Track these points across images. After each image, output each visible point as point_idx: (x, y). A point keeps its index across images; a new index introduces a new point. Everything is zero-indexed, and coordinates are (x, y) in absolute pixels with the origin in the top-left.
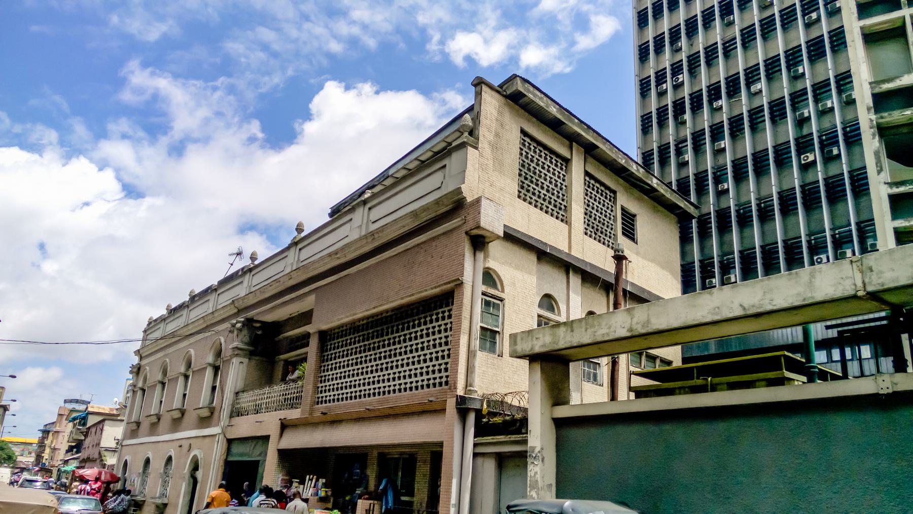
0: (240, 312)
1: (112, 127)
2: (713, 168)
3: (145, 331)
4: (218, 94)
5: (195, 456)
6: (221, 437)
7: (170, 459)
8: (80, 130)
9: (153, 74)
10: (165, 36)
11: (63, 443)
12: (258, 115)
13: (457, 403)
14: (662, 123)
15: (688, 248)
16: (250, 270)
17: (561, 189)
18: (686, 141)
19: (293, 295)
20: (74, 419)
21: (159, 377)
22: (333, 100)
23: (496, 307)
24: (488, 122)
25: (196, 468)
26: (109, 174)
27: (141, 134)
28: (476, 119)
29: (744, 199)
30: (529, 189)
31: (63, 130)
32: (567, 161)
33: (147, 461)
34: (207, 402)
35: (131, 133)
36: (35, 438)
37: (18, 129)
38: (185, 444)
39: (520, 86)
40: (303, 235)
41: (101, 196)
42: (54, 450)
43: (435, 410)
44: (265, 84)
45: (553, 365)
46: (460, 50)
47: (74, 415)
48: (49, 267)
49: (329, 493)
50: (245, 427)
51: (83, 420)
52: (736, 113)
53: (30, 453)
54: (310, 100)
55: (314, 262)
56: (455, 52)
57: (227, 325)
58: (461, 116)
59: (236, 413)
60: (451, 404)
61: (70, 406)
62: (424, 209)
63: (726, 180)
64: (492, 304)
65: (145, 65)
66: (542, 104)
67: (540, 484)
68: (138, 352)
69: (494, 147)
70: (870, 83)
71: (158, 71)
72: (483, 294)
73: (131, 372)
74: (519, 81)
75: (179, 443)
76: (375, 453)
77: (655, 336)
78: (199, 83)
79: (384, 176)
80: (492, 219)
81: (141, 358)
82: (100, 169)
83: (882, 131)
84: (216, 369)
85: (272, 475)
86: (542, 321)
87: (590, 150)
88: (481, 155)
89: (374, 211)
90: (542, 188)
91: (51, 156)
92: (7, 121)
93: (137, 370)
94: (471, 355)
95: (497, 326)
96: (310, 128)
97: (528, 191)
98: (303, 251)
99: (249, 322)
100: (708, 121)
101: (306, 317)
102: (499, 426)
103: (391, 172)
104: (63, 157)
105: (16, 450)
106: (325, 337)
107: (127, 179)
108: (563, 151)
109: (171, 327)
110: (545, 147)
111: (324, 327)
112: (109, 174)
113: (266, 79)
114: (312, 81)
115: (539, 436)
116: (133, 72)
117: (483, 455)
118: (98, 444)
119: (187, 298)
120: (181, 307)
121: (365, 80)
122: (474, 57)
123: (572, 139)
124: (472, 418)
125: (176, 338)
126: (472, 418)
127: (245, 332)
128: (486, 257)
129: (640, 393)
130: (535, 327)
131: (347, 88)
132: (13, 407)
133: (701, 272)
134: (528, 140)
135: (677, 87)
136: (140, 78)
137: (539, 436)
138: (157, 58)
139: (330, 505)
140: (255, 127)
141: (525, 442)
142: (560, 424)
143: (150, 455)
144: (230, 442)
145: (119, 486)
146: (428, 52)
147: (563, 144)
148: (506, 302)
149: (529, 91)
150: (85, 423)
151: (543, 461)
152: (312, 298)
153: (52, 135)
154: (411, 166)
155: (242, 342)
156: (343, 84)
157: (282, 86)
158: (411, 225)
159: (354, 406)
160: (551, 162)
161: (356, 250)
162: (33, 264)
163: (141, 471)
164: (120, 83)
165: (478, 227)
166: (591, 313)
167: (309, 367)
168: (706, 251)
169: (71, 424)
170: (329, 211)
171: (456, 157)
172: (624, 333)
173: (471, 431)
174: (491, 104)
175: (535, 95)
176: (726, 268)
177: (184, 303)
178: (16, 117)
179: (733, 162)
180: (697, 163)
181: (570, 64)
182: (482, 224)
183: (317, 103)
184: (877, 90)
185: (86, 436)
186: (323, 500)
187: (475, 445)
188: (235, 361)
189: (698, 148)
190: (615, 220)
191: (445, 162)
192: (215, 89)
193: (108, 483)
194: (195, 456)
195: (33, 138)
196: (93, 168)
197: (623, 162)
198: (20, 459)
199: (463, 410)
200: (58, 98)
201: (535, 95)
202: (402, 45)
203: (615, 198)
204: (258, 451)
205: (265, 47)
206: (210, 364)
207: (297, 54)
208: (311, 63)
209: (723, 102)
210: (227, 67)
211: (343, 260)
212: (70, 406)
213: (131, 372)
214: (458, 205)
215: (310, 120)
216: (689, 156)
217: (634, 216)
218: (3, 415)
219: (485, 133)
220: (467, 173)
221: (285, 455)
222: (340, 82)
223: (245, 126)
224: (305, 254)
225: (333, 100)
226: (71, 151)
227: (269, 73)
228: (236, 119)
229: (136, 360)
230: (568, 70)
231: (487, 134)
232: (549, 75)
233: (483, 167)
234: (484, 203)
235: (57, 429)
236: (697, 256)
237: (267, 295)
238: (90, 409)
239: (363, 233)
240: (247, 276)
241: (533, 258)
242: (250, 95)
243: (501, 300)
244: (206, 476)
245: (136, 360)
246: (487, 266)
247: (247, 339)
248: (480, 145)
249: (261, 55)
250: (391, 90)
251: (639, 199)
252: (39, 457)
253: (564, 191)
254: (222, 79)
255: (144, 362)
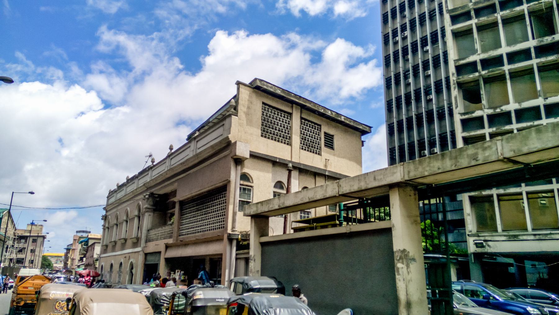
0: (148, 189)
1: (93, 67)
2: (424, 86)
3: (108, 197)
4: (154, 43)
5: (131, 262)
6: (142, 253)
7: (121, 264)
8: (75, 69)
9: (115, 34)
10: (120, 9)
11: (77, 256)
12: (178, 54)
13: (228, 236)
14: (396, 60)
15: (443, 123)
16: (151, 168)
17: (287, 128)
18: (409, 71)
19: (168, 182)
20: (81, 242)
21: (125, 218)
22: (222, 43)
23: (249, 190)
24: (243, 102)
25: (132, 268)
26: (93, 94)
27: (111, 70)
28: (237, 102)
29: (441, 105)
30: (267, 131)
31: (66, 70)
32: (291, 114)
33: (112, 265)
34: (136, 235)
35: (104, 70)
36: (62, 253)
37: (39, 70)
38: (127, 256)
39: (258, 83)
40: (173, 151)
41: (90, 109)
42: (73, 260)
43: (219, 239)
44: (181, 35)
45: (261, 220)
46: (297, 6)
47: (82, 240)
48: (65, 152)
49: (186, 278)
50: (152, 247)
51: (86, 242)
52: (437, 54)
53: (61, 262)
54: (208, 42)
55: (175, 167)
56: (294, 7)
57: (141, 196)
58: (230, 101)
59: (148, 240)
60: (226, 237)
61: (80, 235)
62: (216, 145)
63: (431, 94)
64: (246, 190)
65: (110, 28)
66: (272, 90)
67: (253, 270)
68: (104, 209)
69: (247, 114)
70: (454, 61)
71: (117, 32)
72: (241, 185)
73: (102, 219)
74: (258, 81)
75: (124, 256)
76: (208, 258)
77: (536, 153)
78: (142, 37)
79: (208, 122)
80: (242, 151)
81: (107, 212)
82: (88, 92)
83: (460, 85)
84: (139, 217)
85: (163, 271)
86: (275, 194)
87: (303, 107)
88: (240, 119)
89: (199, 143)
90: (276, 129)
91: (58, 86)
92: (33, 66)
93: (105, 218)
94: (234, 214)
95: (250, 199)
96: (209, 61)
97: (267, 132)
98: (173, 160)
99: (152, 195)
100: (421, 59)
101: (174, 193)
102: (242, 245)
103: (211, 120)
104: (66, 86)
105: (53, 260)
106: (182, 203)
107: (105, 97)
108: (288, 110)
109: (120, 195)
110: (277, 109)
111: (181, 199)
112: (93, 94)
113: (181, 32)
114: (209, 32)
115: (254, 251)
116: (103, 33)
117: (240, 258)
118: (93, 256)
119: (125, 181)
120: (123, 185)
121: (240, 29)
122: (306, 10)
123: (292, 102)
124: (235, 243)
125: (120, 202)
126: (235, 243)
127: (151, 199)
128: (242, 169)
129: (296, 230)
130: (272, 197)
131: (230, 34)
132: (48, 237)
133: (419, 147)
134: (267, 107)
135: (404, 38)
136: (108, 37)
137: (254, 251)
138: (116, 23)
139: (187, 283)
140: (177, 63)
141: (248, 253)
142: (263, 244)
143: (113, 262)
144: (146, 255)
145: (100, 278)
146: (277, 9)
147: (288, 106)
148: (254, 188)
149: (264, 85)
150: (87, 245)
151: (254, 260)
152: (176, 184)
153: (60, 73)
154: (219, 117)
155: (149, 205)
156: (227, 32)
157: (191, 35)
158: (212, 152)
159: (192, 237)
160: (281, 116)
161: (192, 162)
162: (57, 151)
163: (109, 270)
164: (96, 40)
165: (236, 155)
166: (305, 188)
167: (175, 218)
168: (421, 135)
169: (80, 245)
170: (187, 137)
171: (228, 120)
172: (277, 207)
173: (234, 249)
174: (245, 93)
175: (267, 86)
176: (432, 144)
177: (135, 176)
178: (38, 63)
179: (435, 82)
180: (436, 76)
181: (365, 11)
182: (237, 154)
183: (212, 45)
184: (457, 64)
185: (87, 252)
186: (182, 281)
187: (237, 254)
188: (147, 214)
189: (416, 75)
190: (320, 140)
191: (224, 122)
192: (153, 39)
193: (94, 277)
194: (131, 262)
195: (49, 75)
196: (83, 91)
197: (322, 111)
198: (55, 265)
199: (230, 240)
200: (60, 51)
201: (267, 86)
202: (262, 6)
203: (320, 128)
204: (157, 259)
205: (179, 12)
206: (124, 220)
207: (199, 15)
208: (207, 20)
209: (429, 48)
210: (158, 26)
211: (187, 167)
212: (80, 235)
213: (102, 219)
214: (228, 145)
215: (209, 55)
216: (411, 80)
217: (333, 136)
218: (43, 241)
219: (242, 108)
220: (232, 129)
221: (167, 260)
222: (225, 30)
223: (171, 62)
224: (173, 161)
225: (222, 43)
226: (71, 82)
227: (182, 28)
228: (166, 57)
229: (104, 213)
230: (364, 15)
231: (242, 108)
232: (352, 19)
233: (240, 125)
234: (238, 143)
235: (74, 247)
236: (406, 142)
237: (179, 170)
238: (90, 236)
239: (194, 154)
240: (150, 171)
241: (270, 165)
242: (173, 43)
243: (252, 187)
244: (136, 271)
245: (104, 213)
246: (243, 171)
247: (151, 203)
248: (239, 114)
249: (177, 17)
250: (256, 34)
251: (335, 127)
252: (66, 264)
253: (289, 129)
254: (155, 34)
255: (108, 214)
